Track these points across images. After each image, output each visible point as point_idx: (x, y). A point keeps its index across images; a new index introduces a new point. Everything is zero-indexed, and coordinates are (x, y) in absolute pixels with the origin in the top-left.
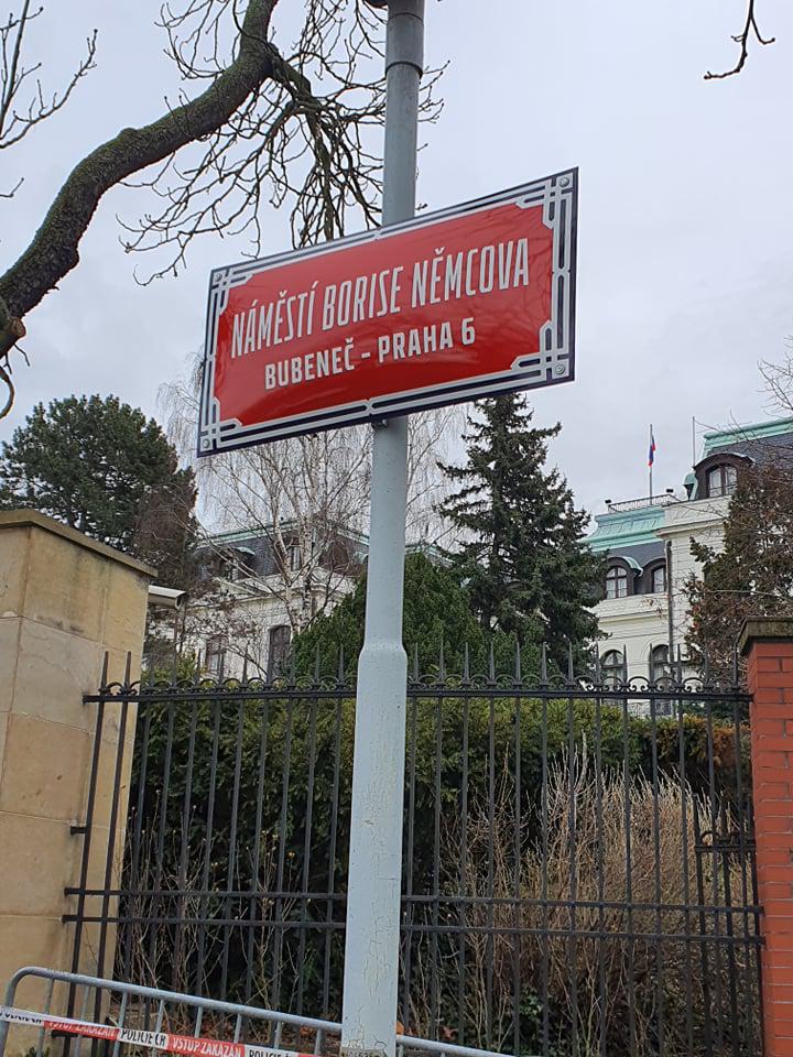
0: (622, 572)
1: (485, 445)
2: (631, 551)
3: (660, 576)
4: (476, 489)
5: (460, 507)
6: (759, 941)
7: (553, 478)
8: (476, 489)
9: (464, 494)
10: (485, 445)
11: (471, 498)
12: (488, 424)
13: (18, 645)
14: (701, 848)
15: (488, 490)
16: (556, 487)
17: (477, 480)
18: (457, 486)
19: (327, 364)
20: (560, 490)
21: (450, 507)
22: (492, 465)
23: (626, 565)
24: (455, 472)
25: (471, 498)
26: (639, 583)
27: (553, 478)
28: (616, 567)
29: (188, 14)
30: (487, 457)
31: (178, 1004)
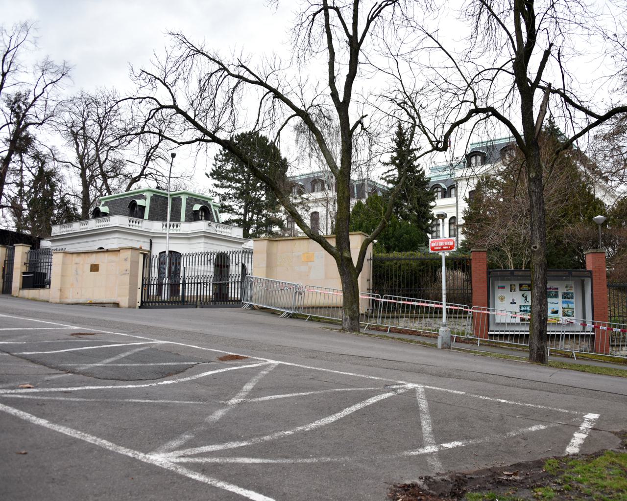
0: (440, 189)
1: (395, 154)
2: (442, 181)
3: (453, 191)
4: (392, 170)
5: (387, 176)
6: (472, 293)
7: (419, 165)
8: (392, 170)
9: (388, 171)
10: (395, 154)
11: (391, 173)
12: (396, 147)
13: (210, 59)
14: (464, 281)
15: (397, 170)
16: (420, 169)
17: (393, 167)
18: (386, 169)
19: (439, 248)
20: (421, 170)
21: (384, 176)
22: (397, 162)
23: (441, 187)
24: (387, 164)
25: (391, 173)
26: (446, 194)
27: (419, 165)
28: (437, 188)
29: (401, 81)
30: (396, 158)
31: (176, 201)
